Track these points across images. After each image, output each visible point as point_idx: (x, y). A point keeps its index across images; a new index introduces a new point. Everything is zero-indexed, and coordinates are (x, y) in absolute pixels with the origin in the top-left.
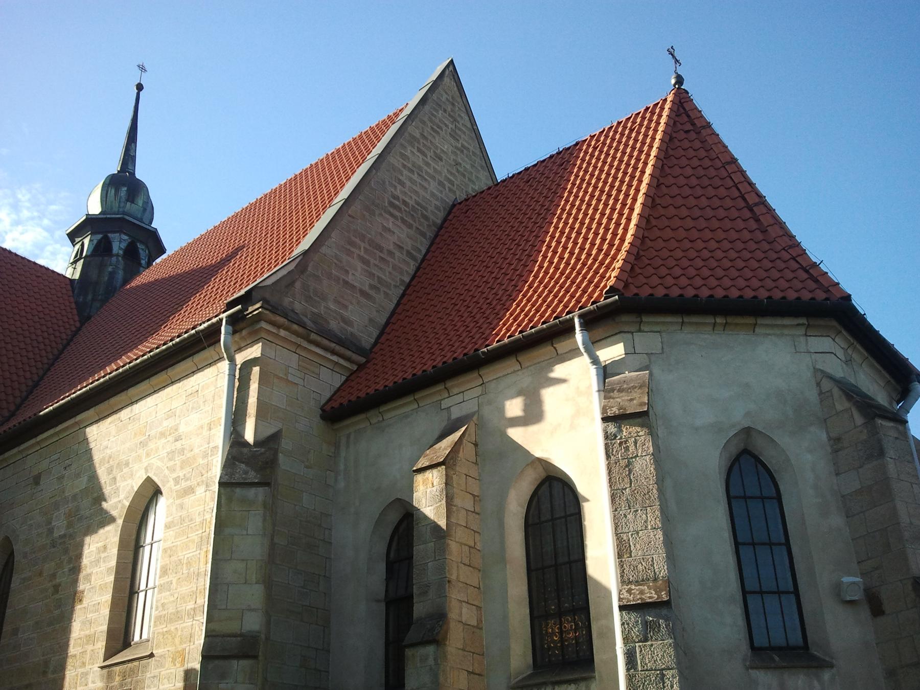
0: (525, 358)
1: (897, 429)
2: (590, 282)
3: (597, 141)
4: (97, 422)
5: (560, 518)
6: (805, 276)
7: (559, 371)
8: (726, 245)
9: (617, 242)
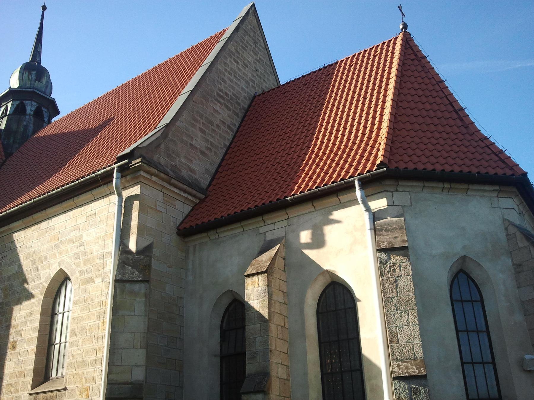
0: (317, 204)
4: (23, 229)
6: (496, 158)
7: (336, 215)
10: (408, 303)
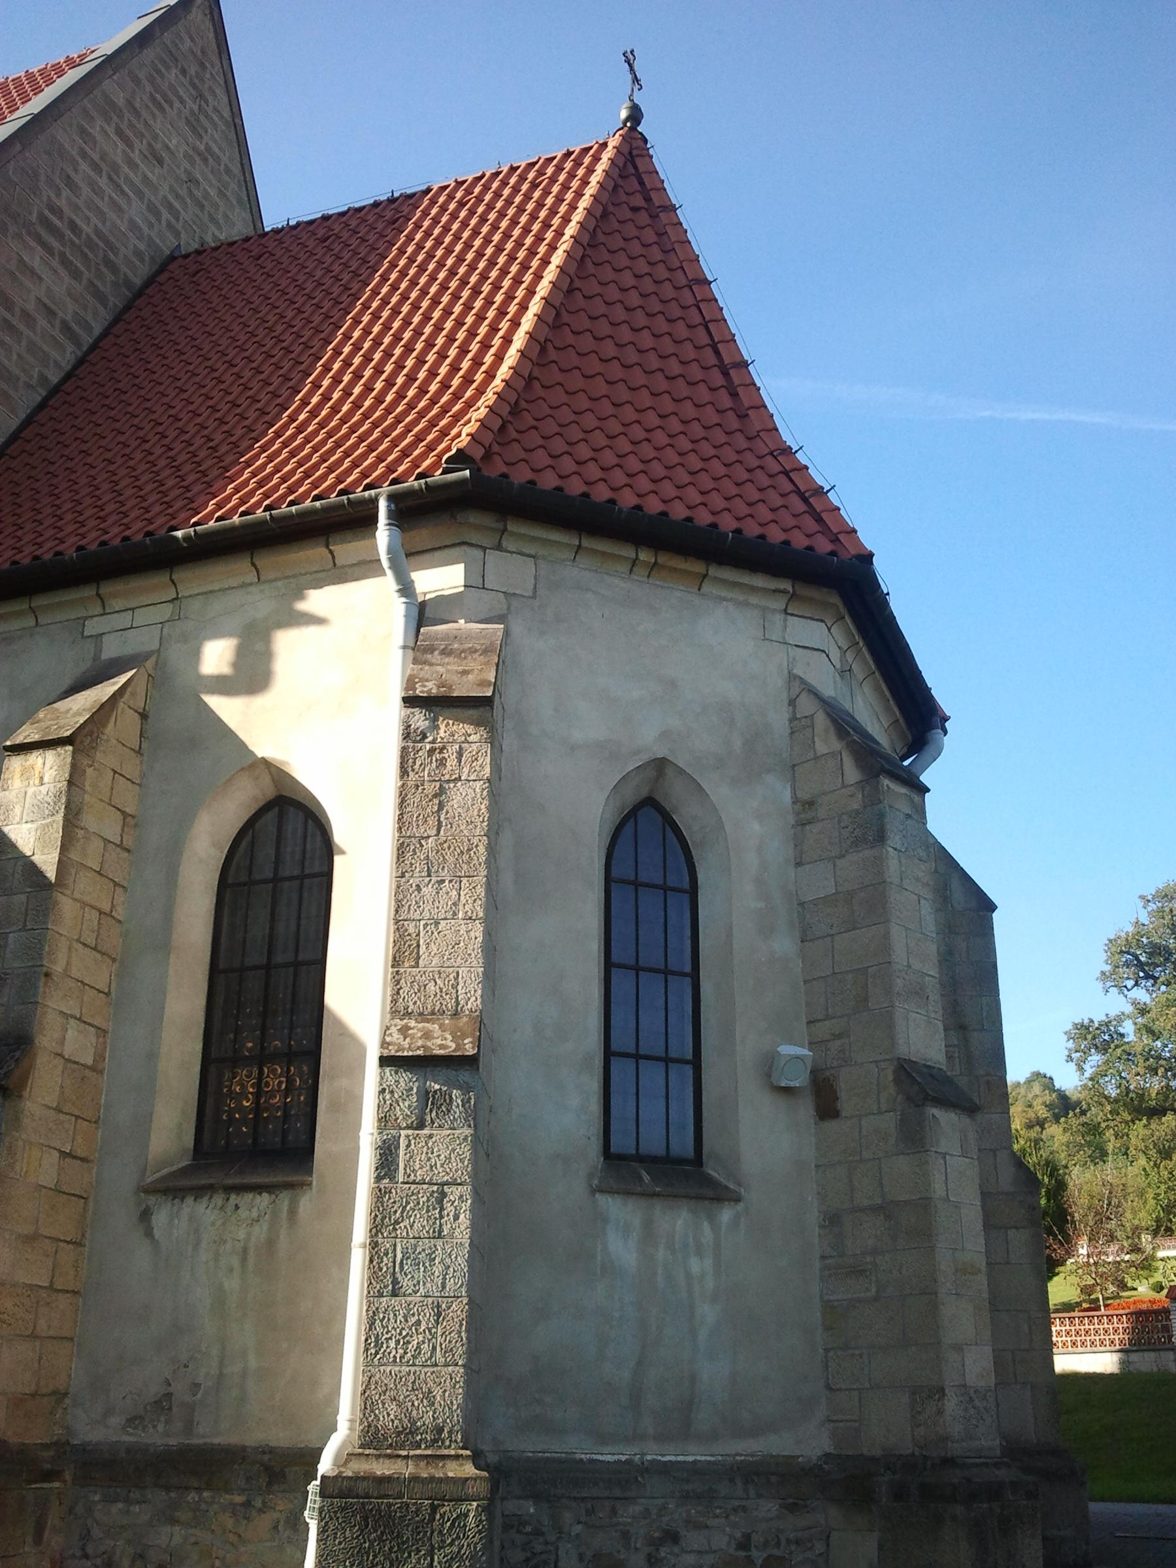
0: (266, 560)
1: (912, 801)
2: (419, 439)
3: (469, 192)
5: (291, 878)
6: (800, 506)
7: (316, 600)
8: (675, 425)
9: (479, 377)
10: (465, 857)
